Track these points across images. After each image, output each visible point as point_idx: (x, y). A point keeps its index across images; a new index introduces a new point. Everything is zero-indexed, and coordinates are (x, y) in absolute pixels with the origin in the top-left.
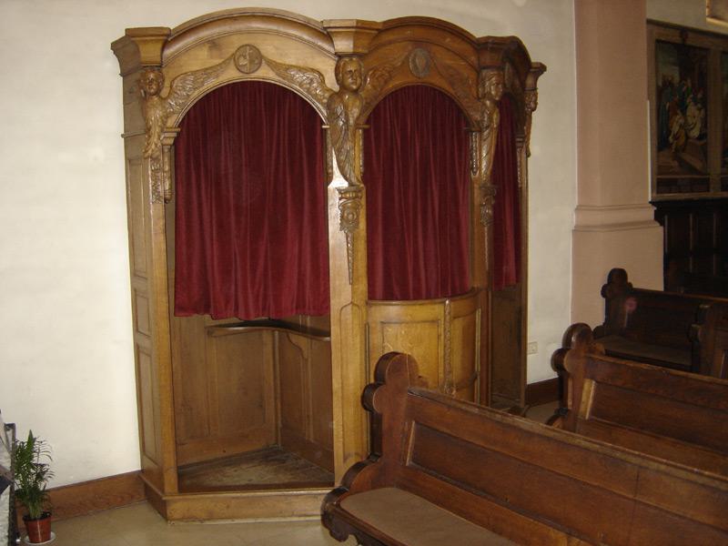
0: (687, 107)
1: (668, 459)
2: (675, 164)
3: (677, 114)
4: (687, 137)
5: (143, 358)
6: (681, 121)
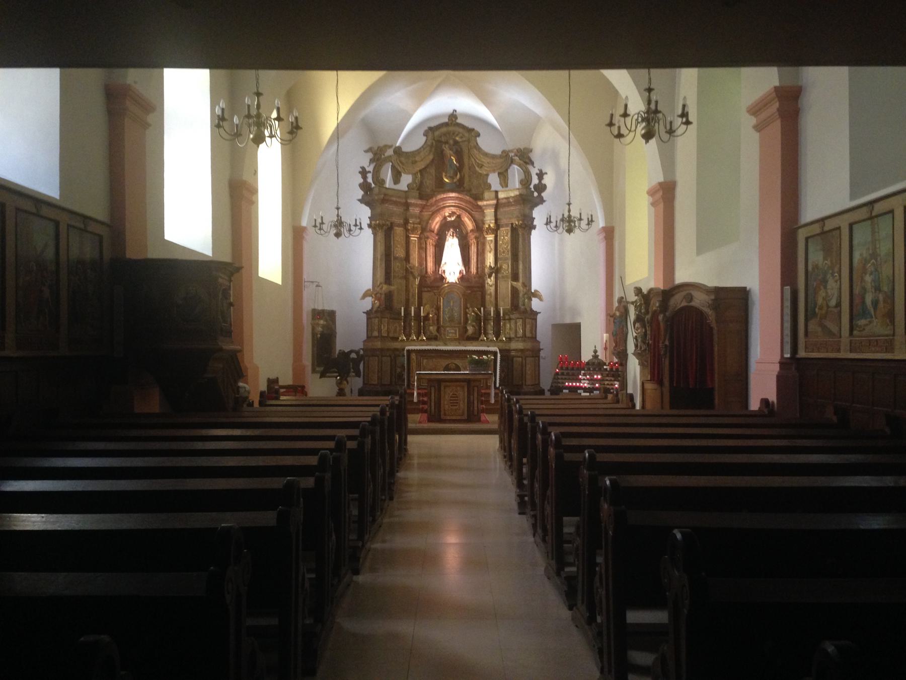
0: (827, 282)
1: (257, 105)
2: (819, 329)
3: (821, 289)
4: (828, 307)
5: (28, 206)
6: (824, 294)
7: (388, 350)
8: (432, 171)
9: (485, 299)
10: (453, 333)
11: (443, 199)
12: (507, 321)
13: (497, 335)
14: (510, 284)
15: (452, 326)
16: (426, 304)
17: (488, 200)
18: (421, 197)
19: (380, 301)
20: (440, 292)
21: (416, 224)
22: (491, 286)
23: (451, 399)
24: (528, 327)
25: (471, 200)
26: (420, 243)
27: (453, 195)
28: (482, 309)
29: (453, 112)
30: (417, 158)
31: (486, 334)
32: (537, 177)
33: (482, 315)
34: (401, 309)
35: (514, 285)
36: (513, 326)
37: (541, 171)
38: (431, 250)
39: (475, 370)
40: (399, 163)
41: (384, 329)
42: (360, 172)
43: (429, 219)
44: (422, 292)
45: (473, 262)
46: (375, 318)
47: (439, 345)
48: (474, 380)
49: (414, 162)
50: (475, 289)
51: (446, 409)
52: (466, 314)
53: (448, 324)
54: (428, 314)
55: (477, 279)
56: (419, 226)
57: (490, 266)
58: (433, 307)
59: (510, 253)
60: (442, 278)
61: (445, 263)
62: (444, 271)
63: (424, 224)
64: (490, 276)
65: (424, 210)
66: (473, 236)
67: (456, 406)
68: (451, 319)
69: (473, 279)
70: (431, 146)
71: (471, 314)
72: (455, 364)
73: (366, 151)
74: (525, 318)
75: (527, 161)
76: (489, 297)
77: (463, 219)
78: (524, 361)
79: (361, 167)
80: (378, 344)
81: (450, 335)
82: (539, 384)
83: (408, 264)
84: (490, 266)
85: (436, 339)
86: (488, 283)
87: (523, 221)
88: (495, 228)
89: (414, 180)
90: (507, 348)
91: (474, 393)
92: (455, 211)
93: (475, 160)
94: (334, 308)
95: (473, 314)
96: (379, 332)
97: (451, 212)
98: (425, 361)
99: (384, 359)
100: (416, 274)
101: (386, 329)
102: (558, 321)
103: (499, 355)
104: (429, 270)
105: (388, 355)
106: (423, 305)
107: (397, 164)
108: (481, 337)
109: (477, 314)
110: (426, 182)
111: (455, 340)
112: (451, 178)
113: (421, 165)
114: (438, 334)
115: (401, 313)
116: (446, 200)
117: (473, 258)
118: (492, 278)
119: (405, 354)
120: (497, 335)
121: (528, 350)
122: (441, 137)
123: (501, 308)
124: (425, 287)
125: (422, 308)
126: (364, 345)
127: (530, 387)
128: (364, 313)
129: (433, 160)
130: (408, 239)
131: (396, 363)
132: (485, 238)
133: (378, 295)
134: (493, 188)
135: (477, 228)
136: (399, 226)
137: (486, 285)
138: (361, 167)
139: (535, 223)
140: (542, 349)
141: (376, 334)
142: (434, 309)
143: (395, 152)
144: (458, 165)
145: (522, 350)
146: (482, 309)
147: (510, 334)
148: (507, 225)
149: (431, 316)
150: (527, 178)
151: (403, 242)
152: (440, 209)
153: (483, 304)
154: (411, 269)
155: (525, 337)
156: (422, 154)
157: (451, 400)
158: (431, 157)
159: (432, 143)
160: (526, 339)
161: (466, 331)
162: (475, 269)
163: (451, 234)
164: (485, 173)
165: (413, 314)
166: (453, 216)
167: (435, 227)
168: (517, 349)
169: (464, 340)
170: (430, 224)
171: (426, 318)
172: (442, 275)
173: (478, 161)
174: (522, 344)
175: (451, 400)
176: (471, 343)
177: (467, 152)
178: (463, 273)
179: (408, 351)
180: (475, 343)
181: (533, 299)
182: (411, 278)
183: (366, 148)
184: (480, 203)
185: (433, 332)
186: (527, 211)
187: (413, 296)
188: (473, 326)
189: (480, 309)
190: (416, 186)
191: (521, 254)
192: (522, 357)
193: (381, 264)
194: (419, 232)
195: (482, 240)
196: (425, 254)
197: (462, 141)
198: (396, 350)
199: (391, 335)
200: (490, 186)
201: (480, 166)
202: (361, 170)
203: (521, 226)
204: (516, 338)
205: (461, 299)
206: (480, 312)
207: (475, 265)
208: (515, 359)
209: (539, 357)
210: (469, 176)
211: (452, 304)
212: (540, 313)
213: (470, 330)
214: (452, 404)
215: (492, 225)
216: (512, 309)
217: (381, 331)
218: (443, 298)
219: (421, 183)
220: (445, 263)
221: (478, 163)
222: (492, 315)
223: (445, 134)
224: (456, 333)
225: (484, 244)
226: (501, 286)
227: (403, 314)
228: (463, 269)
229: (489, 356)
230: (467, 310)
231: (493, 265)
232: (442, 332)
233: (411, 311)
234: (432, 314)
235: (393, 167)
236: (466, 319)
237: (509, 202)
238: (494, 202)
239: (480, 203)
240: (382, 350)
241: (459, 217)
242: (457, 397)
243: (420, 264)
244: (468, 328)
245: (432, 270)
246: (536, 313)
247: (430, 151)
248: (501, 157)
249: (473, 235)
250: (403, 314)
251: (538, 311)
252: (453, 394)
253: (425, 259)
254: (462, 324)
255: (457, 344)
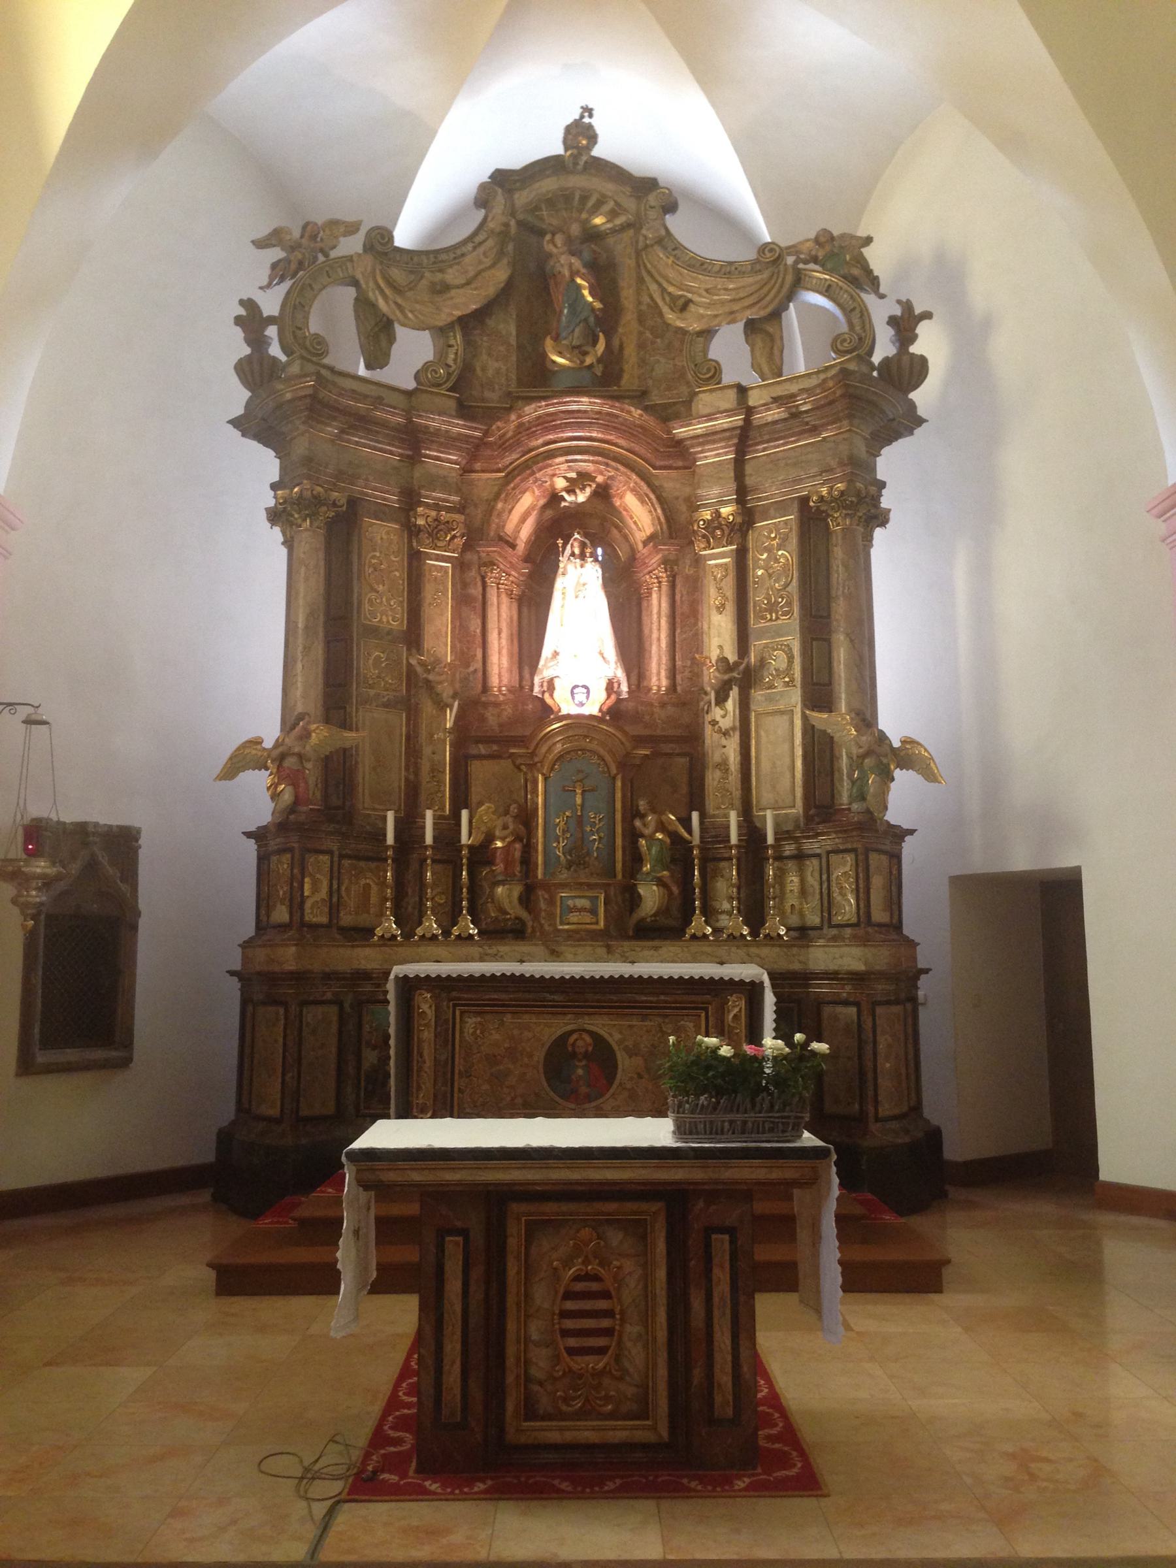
7: (329, 977)
8: (507, 326)
9: (702, 779)
10: (581, 910)
11: (546, 424)
12: (791, 864)
13: (755, 915)
14: (798, 723)
15: (581, 884)
16: (480, 804)
17: (710, 417)
18: (465, 411)
19: (295, 785)
20: (533, 754)
21: (449, 510)
22: (726, 734)
23: (570, 1305)
24: (877, 882)
25: (650, 421)
26: (462, 585)
27: (583, 403)
28: (695, 816)
29: (582, 117)
30: (452, 276)
31: (709, 913)
32: (891, 331)
33: (696, 840)
34: (384, 818)
35: (819, 726)
36: (812, 881)
37: (907, 306)
38: (505, 614)
39: (714, 1132)
40: (382, 284)
41: (315, 893)
42: (238, 321)
43: (497, 497)
44: (467, 757)
45: (654, 648)
46: (281, 851)
47: (532, 958)
48: (715, 1193)
49: (441, 289)
50: (667, 748)
51: (534, 1372)
52: (633, 836)
53: (564, 876)
54: (490, 838)
55: (670, 710)
56: (460, 518)
57: (723, 660)
58: (507, 813)
59: (796, 609)
60: (546, 711)
61: (556, 654)
62: (551, 685)
63: (478, 513)
64: (721, 700)
65: (478, 466)
66: (657, 558)
67: (602, 1351)
68: (578, 857)
69: (657, 710)
70: (503, 235)
71: (651, 838)
72: (592, 1034)
73: (260, 244)
74: (867, 851)
75: (856, 272)
76: (718, 774)
77: (617, 502)
78: (868, 1025)
79: (242, 303)
80: (288, 957)
81: (574, 917)
82: (917, 1108)
83: (414, 651)
84: (723, 660)
85: (517, 932)
86: (714, 723)
87: (850, 480)
88: (739, 520)
89: (441, 355)
90: (796, 967)
91: (708, 1271)
92: (589, 467)
93: (660, 285)
94: (136, 824)
95: (659, 836)
96: (291, 907)
97: (574, 475)
98: (471, 1021)
99: (312, 1015)
100: (445, 690)
101: (323, 893)
102: (979, 863)
103: (769, 999)
104: (494, 681)
105: (329, 996)
106: (474, 798)
107: (371, 284)
108: (462, 923)
109: (675, 837)
110: (484, 369)
111: (594, 936)
112: (579, 351)
113: (466, 302)
114: (524, 915)
115: (385, 835)
116: (556, 428)
117: (655, 635)
118: (730, 704)
119: (391, 997)
120: (755, 915)
121: (882, 976)
122: (537, 208)
123: (769, 815)
124: (479, 741)
125: (465, 814)
126: (246, 959)
127: (894, 1125)
128: (248, 835)
129: (507, 290)
130: (415, 559)
131: (360, 1026)
132: (698, 561)
133: (290, 762)
134: (728, 378)
135: (669, 527)
136: (381, 513)
137: (708, 730)
138: (242, 303)
139: (885, 503)
140: (927, 971)
141: (281, 914)
142: (509, 820)
143: (369, 247)
144: (598, 305)
145: (857, 978)
146: (695, 816)
147: (802, 915)
148: (781, 507)
149: (499, 844)
150: (858, 328)
151: (399, 575)
152: (536, 460)
153: (696, 798)
154: (429, 671)
155: (869, 922)
156: (470, 262)
157: (564, 1314)
158: (501, 274)
159: (507, 225)
160: (870, 930)
161: (634, 900)
162: (663, 673)
163: (577, 551)
164: (696, 326)
165: (429, 839)
166: (583, 489)
167: (518, 530)
168: (836, 973)
169: (629, 938)
170: (499, 515)
171: (481, 854)
172: (542, 700)
173: (671, 289)
174: (857, 951)
175: (564, 1314)
176: (656, 948)
177: (631, 262)
178: (619, 693)
179: (409, 986)
180: (669, 948)
181: (898, 773)
182: (428, 708)
183: (263, 231)
184: (681, 431)
185: (507, 906)
186: (861, 450)
187: (436, 771)
188: (660, 882)
189: (690, 819)
190: (449, 374)
191: (840, 608)
192: (857, 1004)
193: (307, 649)
194: (460, 542)
195: (689, 571)
196: (479, 622)
197: (615, 231)
198: (363, 976)
199: (346, 919)
200: (714, 373)
201: (681, 302)
202: (242, 312)
203: (840, 501)
204: (831, 926)
205: (614, 778)
206: (689, 830)
207: (664, 660)
208: (827, 1010)
209: (913, 1000)
210: (641, 346)
211: (579, 800)
212: (911, 832)
213: (651, 896)
214: (572, 1342)
215: (726, 511)
216: (808, 818)
217: (302, 903)
218: (546, 779)
219: (467, 369)
220: (556, 654)
221: (670, 294)
222: (734, 839)
223: (550, 202)
224: (593, 912)
225: (695, 585)
226: (764, 739)
227: (390, 839)
228: (620, 674)
229: (799, 1037)
230: (638, 823)
231: (732, 657)
232: (543, 905)
233: (423, 827)
234: (502, 839)
235: (363, 305)
236: (635, 859)
237: (795, 415)
238: (738, 419)
239: (681, 431)
240: (299, 977)
241: (603, 494)
242: (606, 1295)
243: (464, 658)
244: (641, 891)
245: (505, 681)
246: (899, 834)
247: (501, 253)
248: (755, 266)
249: (659, 552)
250: (390, 839)
251: (905, 827)
252: (577, 1278)
253: (479, 640)
254: (620, 876)
255: (601, 951)
